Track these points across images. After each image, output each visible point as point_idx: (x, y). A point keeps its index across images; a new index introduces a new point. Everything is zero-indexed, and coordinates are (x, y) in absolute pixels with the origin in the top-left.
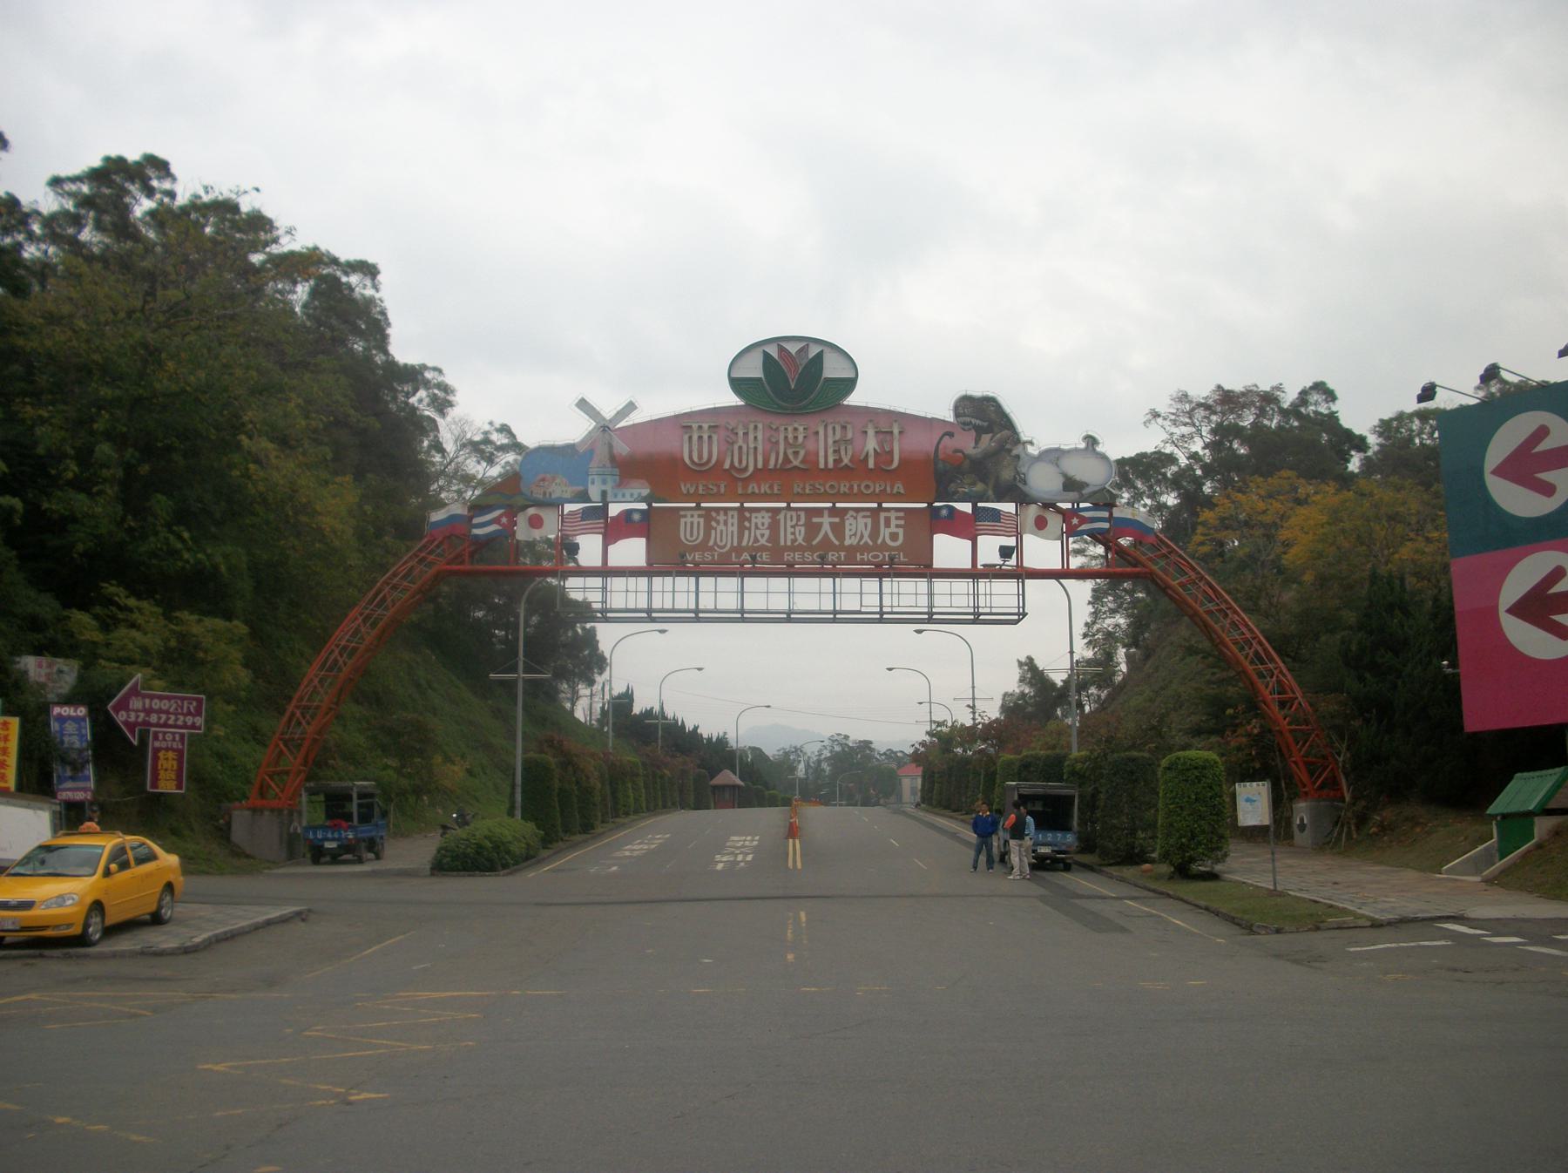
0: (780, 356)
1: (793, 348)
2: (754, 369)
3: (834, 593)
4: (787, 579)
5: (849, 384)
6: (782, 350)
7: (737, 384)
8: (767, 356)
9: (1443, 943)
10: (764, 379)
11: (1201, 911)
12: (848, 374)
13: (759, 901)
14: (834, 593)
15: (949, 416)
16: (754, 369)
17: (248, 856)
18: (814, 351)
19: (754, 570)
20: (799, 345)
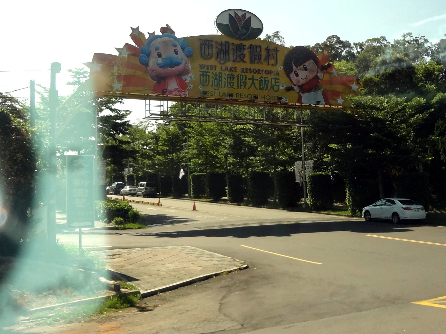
0: (235, 16)
1: (240, 14)
2: (226, 22)
3: (160, 105)
4: (167, 102)
5: (260, 31)
6: (236, 14)
7: (219, 26)
8: (230, 15)
9: (82, 270)
10: (229, 25)
11: (179, 262)
12: (259, 27)
13: (199, 283)
14: (160, 105)
15: (214, 31)
16: (226, 22)
17: (221, 287)
18: (247, 16)
19: (185, 99)
20: (243, 13)
